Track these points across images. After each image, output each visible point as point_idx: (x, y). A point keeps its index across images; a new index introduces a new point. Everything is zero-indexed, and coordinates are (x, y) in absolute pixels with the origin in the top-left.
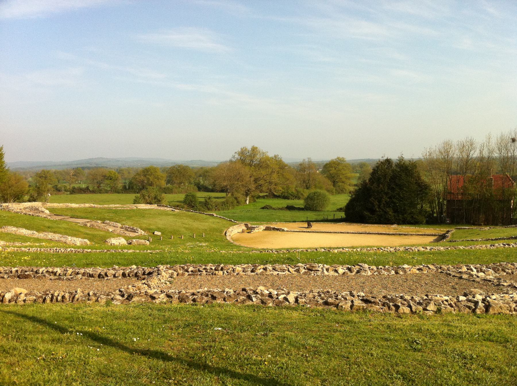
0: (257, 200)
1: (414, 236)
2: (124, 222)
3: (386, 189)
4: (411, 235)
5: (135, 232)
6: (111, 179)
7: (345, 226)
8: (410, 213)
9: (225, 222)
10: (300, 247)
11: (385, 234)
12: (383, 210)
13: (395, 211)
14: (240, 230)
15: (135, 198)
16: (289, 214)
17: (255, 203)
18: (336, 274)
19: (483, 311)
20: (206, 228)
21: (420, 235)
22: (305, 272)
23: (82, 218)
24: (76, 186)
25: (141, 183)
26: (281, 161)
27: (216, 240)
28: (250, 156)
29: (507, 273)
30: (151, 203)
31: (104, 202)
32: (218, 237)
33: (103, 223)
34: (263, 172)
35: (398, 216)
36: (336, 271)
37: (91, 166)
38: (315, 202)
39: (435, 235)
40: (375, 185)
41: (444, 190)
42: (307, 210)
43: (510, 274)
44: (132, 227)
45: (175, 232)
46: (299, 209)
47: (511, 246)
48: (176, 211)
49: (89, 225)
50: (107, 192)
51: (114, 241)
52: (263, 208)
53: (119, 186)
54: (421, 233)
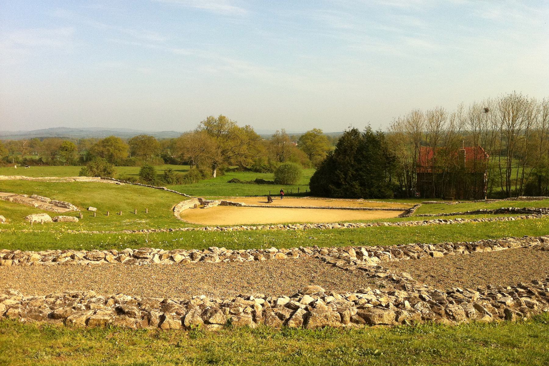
0: (225, 173)
1: (379, 211)
2: (55, 197)
3: (352, 161)
4: (376, 210)
5: (66, 207)
6: (66, 150)
7: (308, 201)
8: (377, 187)
9: (175, 196)
10: (231, 223)
11: (349, 209)
12: (348, 183)
13: (362, 184)
14: (192, 205)
15: (81, 170)
16: (256, 188)
17: (223, 177)
18: (172, 262)
19: (300, 323)
20: (152, 203)
21: (385, 210)
22: (129, 261)
23: (6, 192)
24: (28, 157)
25: (98, 155)
26: (252, 132)
27: (160, 217)
28: (218, 126)
29: (411, 258)
31: (37, 175)
32: (163, 215)
33: (30, 197)
34: (231, 143)
35: (365, 190)
36: (172, 258)
37: (51, 136)
38: (286, 175)
39: (401, 210)
40: (341, 156)
41: (414, 163)
42: (277, 184)
43: (415, 259)
44: (62, 202)
45: (114, 208)
46: (269, 183)
47: (449, 223)
48: (121, 184)
49: (11, 199)
50: (62, 164)
51: (35, 218)
52: (230, 182)
53: (76, 158)
54: (386, 208)
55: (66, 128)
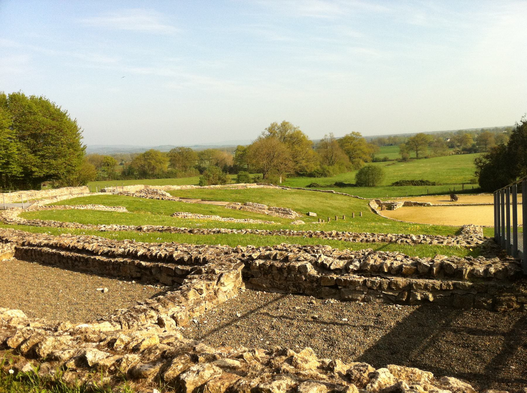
6: (108, 165)
30: (216, 184)
52: (309, 186)
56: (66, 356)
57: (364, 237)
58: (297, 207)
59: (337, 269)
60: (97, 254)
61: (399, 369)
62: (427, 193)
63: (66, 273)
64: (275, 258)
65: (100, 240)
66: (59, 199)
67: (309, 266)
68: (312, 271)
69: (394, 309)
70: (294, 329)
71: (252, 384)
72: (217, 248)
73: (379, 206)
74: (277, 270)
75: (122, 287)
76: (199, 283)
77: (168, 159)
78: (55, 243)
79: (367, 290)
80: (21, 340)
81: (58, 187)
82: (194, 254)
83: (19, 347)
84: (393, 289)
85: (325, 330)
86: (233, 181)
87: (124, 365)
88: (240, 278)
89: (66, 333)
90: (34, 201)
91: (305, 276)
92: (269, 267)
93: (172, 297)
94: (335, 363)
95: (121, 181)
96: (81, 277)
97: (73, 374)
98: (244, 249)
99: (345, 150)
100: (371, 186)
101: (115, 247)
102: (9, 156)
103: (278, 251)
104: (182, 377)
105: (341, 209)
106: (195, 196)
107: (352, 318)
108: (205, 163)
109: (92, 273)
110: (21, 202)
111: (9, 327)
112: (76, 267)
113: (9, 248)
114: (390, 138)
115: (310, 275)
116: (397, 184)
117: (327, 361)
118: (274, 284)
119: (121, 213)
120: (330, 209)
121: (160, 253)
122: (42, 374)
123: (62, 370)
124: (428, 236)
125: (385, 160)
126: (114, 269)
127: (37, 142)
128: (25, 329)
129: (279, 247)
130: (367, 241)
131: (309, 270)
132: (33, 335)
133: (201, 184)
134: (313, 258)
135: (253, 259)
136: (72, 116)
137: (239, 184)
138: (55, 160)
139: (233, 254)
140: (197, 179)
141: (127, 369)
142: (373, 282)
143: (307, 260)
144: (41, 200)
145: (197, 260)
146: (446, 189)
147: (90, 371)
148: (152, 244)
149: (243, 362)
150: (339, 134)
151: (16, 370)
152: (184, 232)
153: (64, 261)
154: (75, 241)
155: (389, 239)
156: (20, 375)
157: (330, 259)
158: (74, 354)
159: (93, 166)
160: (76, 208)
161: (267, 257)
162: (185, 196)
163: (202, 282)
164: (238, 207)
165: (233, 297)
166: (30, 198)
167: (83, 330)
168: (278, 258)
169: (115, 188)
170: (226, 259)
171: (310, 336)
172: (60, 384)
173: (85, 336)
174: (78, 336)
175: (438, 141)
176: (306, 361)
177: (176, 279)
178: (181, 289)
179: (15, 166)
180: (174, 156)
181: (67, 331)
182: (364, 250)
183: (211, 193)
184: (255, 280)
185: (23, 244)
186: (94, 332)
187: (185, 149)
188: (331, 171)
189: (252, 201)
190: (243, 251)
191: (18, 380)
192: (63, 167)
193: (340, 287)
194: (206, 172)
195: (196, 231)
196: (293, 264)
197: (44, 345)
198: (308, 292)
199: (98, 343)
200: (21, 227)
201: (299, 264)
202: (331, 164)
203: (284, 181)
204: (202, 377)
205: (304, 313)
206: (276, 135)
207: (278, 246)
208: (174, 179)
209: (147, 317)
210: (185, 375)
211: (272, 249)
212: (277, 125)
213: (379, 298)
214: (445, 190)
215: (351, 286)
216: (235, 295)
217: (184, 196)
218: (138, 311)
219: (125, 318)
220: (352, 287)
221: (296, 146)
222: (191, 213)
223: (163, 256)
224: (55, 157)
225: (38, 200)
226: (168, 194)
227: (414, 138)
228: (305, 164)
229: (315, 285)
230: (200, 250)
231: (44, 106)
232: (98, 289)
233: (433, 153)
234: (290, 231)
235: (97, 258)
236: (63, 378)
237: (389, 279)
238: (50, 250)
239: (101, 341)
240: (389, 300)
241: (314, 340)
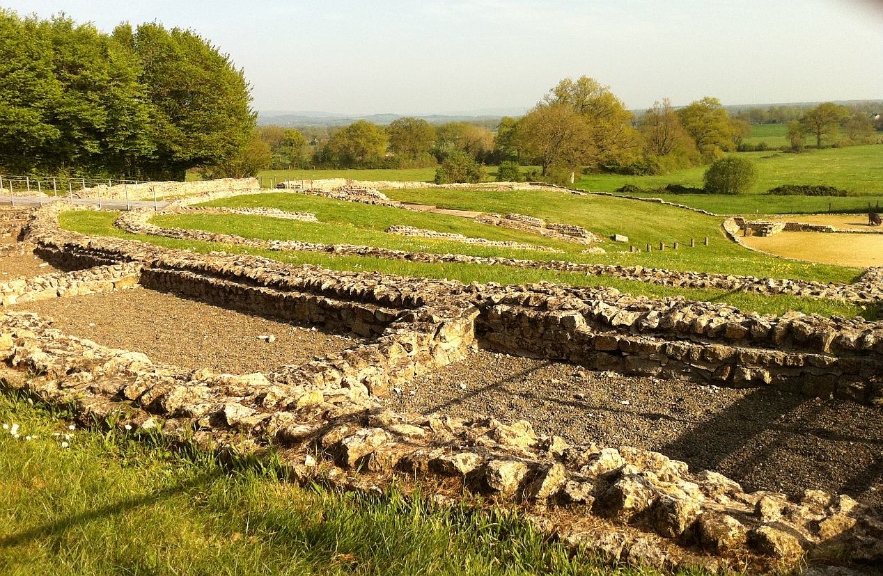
6: (291, 145)
52: (622, 190)
55: (448, 117)
56: (199, 411)
57: (687, 279)
58: (594, 225)
59: (621, 326)
60: (261, 284)
61: (635, 452)
62: (827, 210)
63: (214, 311)
64: (526, 304)
65: (268, 263)
66: (212, 197)
67: (579, 318)
68: (582, 326)
69: (706, 392)
70: (543, 410)
71: (431, 455)
72: (441, 284)
73: (741, 229)
74: (529, 322)
75: (296, 335)
76: (407, 334)
77: (387, 137)
78: (201, 266)
79: (667, 360)
80: (142, 389)
81: (211, 178)
82: (406, 291)
83: (139, 398)
84: (708, 361)
85: (591, 415)
86: (491, 178)
87: (273, 425)
88: (472, 332)
89: (202, 384)
90: (173, 199)
91: (572, 334)
92: (517, 317)
93: (364, 353)
94: (552, 440)
95: (311, 171)
96: (237, 318)
97: (207, 434)
98: (482, 287)
99: (689, 130)
100: (730, 194)
101: (289, 275)
102: (136, 126)
103: (532, 293)
104: (343, 442)
105: (672, 232)
106: (425, 200)
107: (637, 401)
108: (447, 144)
109: (253, 313)
110: (153, 200)
111: (127, 373)
112: (231, 303)
113: (133, 270)
114: (772, 109)
115: (578, 332)
116: (778, 191)
117: (544, 437)
118: (524, 343)
119: (306, 223)
120: (653, 231)
121: (355, 287)
122: (167, 433)
123: (193, 428)
124: (796, 282)
125: (761, 148)
126: (286, 308)
127: (180, 105)
128: (148, 375)
129: (536, 286)
130: (692, 285)
131: (577, 324)
132: (158, 383)
133: (437, 181)
134: (586, 306)
135: (493, 304)
136: (237, 61)
137: (501, 183)
138: (207, 134)
139: (464, 294)
140: (431, 172)
141: (276, 431)
142: (677, 349)
143: (576, 309)
144: (185, 197)
145: (408, 302)
146: (862, 202)
147: (228, 431)
148: (344, 273)
149: (429, 431)
150: (681, 100)
151: (135, 427)
152: (399, 258)
153: (214, 292)
154: (231, 263)
155: (730, 283)
156: (138, 432)
157: (613, 310)
158: (209, 410)
159: (267, 146)
160: (238, 212)
161: (513, 302)
162: (409, 199)
163: (412, 333)
164: (495, 221)
165: (458, 360)
166: (168, 194)
167: (225, 381)
168: (530, 304)
169: (299, 183)
170: (451, 302)
171: (567, 422)
172: (190, 444)
173: (227, 388)
174: (218, 388)
175: (859, 118)
176: (514, 436)
177: (376, 328)
178: (379, 342)
179: (146, 142)
180: (397, 133)
181: (203, 381)
182: (670, 298)
183: (453, 197)
184: (494, 336)
185: (153, 265)
186: (239, 384)
187: (416, 121)
188: (662, 166)
189: (519, 212)
190: (480, 290)
191: (136, 439)
192: (220, 145)
193: (624, 354)
194: (447, 160)
195: (416, 257)
196: (554, 313)
197: (172, 397)
198: (575, 358)
199: (243, 398)
200: (151, 238)
201: (564, 314)
202: (663, 152)
203: (578, 180)
204: (370, 444)
205: (563, 389)
206: (569, 100)
207: (534, 285)
208: (394, 171)
209: (326, 378)
210: (347, 440)
211: (525, 289)
212: (570, 82)
213: (685, 374)
214: (862, 206)
215: (642, 353)
216: (461, 357)
217: (408, 199)
218: (313, 369)
219: (294, 378)
220: (643, 355)
221: (601, 121)
222: (418, 228)
223: (359, 291)
224: (208, 130)
225: (179, 197)
226: (383, 196)
227: (816, 111)
228: (617, 151)
229: (586, 348)
230: (415, 286)
231: (190, 43)
232: (260, 337)
233: (848, 139)
234: (566, 263)
235: (262, 290)
236: (194, 438)
237: (703, 345)
238: (194, 276)
239: (247, 395)
240: (700, 378)
241: (571, 429)
